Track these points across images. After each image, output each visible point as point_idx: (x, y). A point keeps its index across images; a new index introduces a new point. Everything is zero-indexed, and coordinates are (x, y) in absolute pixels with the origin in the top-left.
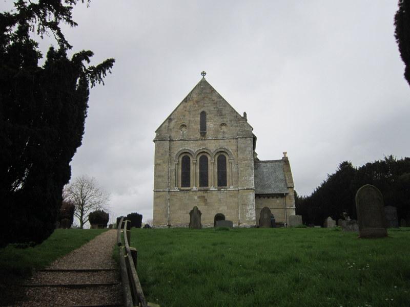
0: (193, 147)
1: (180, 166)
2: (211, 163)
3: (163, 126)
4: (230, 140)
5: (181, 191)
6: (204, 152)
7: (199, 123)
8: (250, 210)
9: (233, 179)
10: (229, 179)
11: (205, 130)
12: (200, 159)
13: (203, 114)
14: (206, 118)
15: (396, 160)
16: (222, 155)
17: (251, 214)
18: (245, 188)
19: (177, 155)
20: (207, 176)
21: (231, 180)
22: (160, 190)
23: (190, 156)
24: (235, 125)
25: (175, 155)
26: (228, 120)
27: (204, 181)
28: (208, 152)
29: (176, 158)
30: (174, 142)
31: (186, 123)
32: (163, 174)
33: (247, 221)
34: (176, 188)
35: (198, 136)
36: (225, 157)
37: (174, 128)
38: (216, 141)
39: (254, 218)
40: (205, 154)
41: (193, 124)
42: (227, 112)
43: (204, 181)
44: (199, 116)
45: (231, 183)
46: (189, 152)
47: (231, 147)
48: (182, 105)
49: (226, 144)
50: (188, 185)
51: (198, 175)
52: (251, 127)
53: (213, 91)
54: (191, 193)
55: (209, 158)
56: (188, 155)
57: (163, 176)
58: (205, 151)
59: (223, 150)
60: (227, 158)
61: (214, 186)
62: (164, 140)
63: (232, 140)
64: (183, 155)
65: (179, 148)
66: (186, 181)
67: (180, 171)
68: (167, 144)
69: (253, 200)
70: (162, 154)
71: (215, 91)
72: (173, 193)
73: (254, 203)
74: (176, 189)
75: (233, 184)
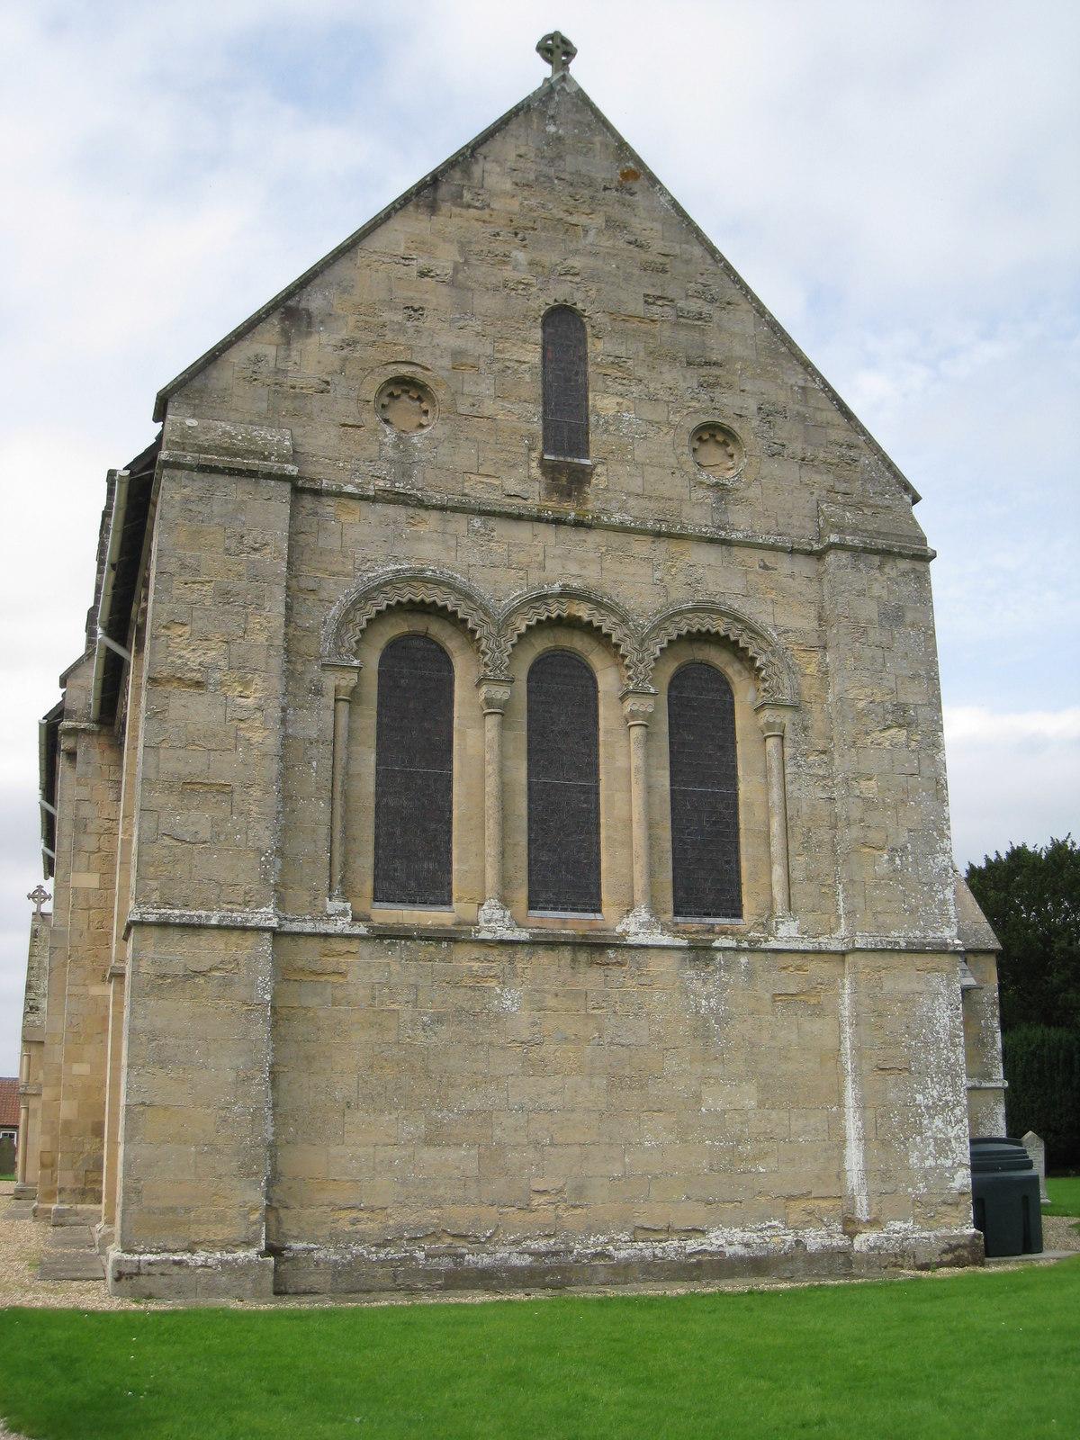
0: (506, 570)
1: (368, 719)
2: (628, 721)
3: (237, 356)
4: (769, 558)
5: (386, 936)
6: (572, 624)
7: (530, 385)
8: (933, 1110)
9: (799, 862)
10: (763, 868)
11: (580, 446)
12: (532, 672)
13: (563, 325)
14: (583, 359)
15: (1004, 856)
16: (708, 667)
17: (943, 1147)
18: (899, 936)
19: (344, 621)
20: (587, 821)
21: (778, 872)
22: (196, 914)
23: (453, 644)
24: (796, 447)
25: (335, 611)
26: (752, 405)
27: (561, 861)
28: (606, 623)
29: (338, 636)
30: (329, 507)
31: (435, 368)
32: (226, 768)
33: (918, 1201)
34: (334, 906)
35: (524, 482)
36: (725, 688)
37: (324, 388)
38: (663, 546)
39: (1043, 1216)
40: (579, 643)
41: (486, 387)
42: (739, 350)
43: (561, 861)
44: (538, 335)
45: (779, 894)
46: (450, 602)
47: (776, 605)
48: (395, 223)
49: (737, 585)
50: (436, 889)
51: (521, 805)
52: (907, 487)
53: (630, 175)
54: (466, 960)
55: (608, 680)
56: (437, 629)
57: (224, 790)
58: (583, 611)
59: (720, 626)
60: (744, 695)
61: (505, 902)
62: (251, 474)
63: (784, 564)
64: (397, 628)
65: (370, 549)
66: (412, 851)
67: (367, 761)
68: (49, 1171)
69: (953, 1036)
70: (225, 595)
71: (653, 180)
72: (307, 954)
73: (961, 1055)
74: (338, 916)
75: (798, 901)
